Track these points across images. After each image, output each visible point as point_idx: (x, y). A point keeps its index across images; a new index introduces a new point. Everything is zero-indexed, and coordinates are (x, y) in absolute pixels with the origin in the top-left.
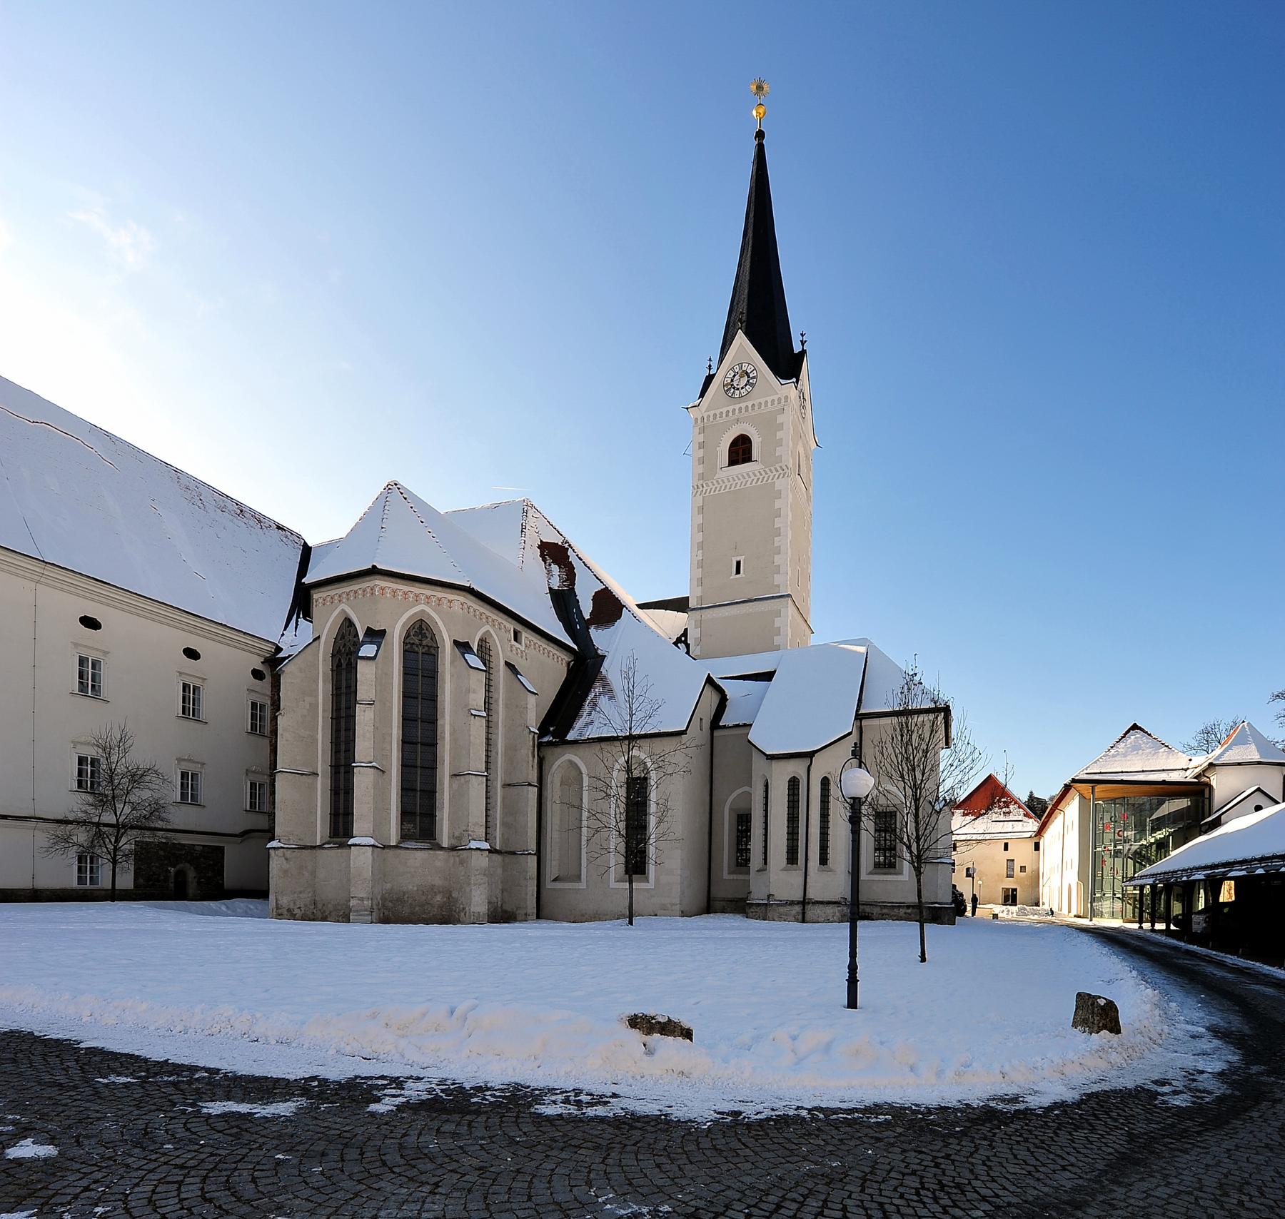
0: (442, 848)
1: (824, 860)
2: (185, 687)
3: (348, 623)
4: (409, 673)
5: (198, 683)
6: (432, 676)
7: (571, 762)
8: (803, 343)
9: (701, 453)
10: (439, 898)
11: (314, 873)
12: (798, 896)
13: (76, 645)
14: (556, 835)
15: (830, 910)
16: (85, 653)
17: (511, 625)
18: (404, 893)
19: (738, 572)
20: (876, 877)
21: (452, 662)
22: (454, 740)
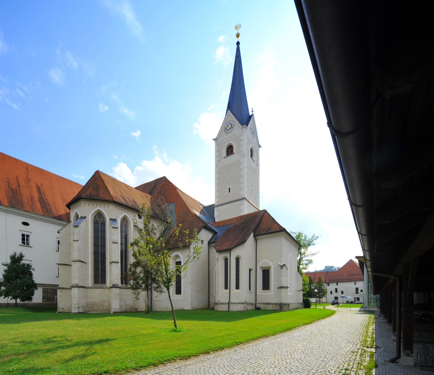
1: (237, 287)
2: (23, 235)
4: (96, 230)
5: (28, 234)
6: (104, 231)
8: (252, 111)
12: (232, 300)
16: (24, 233)
18: (94, 302)
20: (262, 294)
21: (133, 231)
22: (110, 249)
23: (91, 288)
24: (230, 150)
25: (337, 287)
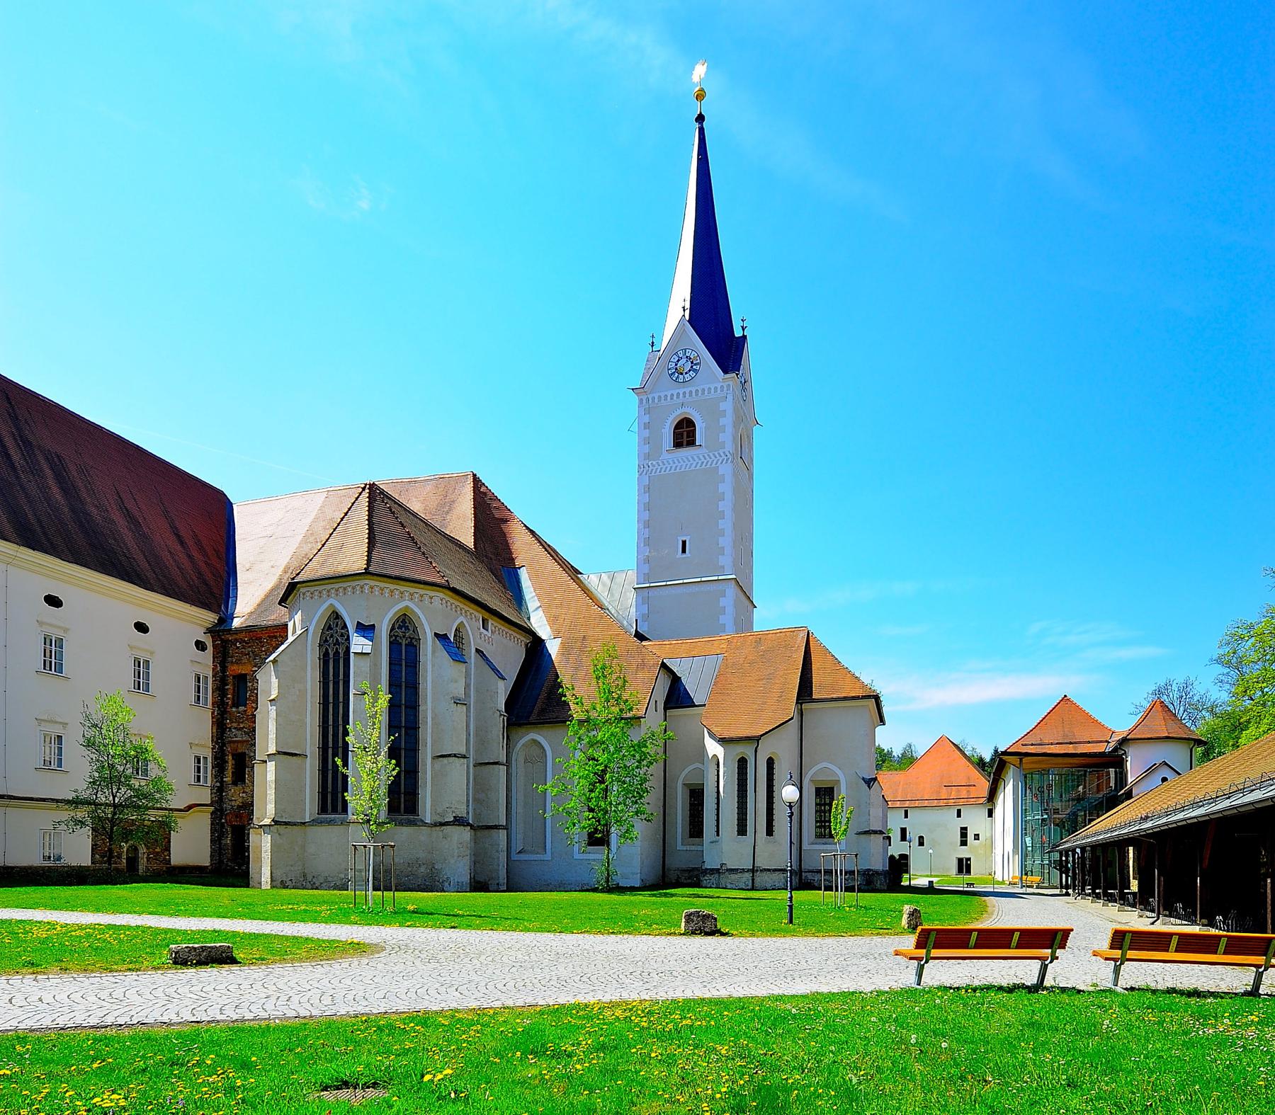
0: (425, 824)
1: (770, 832)
3: (336, 616)
5: (60, 634)
7: (535, 741)
9: (646, 433)
10: (422, 869)
11: (303, 847)
13: (131, 647)
14: (520, 810)
15: (777, 877)
17: (479, 614)
19: (684, 551)
21: (434, 652)
23: (314, 822)
24: (684, 434)
25: (904, 823)
